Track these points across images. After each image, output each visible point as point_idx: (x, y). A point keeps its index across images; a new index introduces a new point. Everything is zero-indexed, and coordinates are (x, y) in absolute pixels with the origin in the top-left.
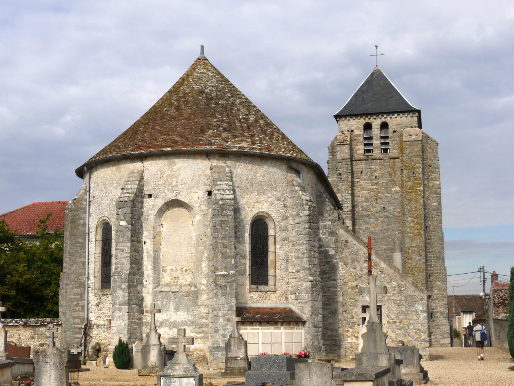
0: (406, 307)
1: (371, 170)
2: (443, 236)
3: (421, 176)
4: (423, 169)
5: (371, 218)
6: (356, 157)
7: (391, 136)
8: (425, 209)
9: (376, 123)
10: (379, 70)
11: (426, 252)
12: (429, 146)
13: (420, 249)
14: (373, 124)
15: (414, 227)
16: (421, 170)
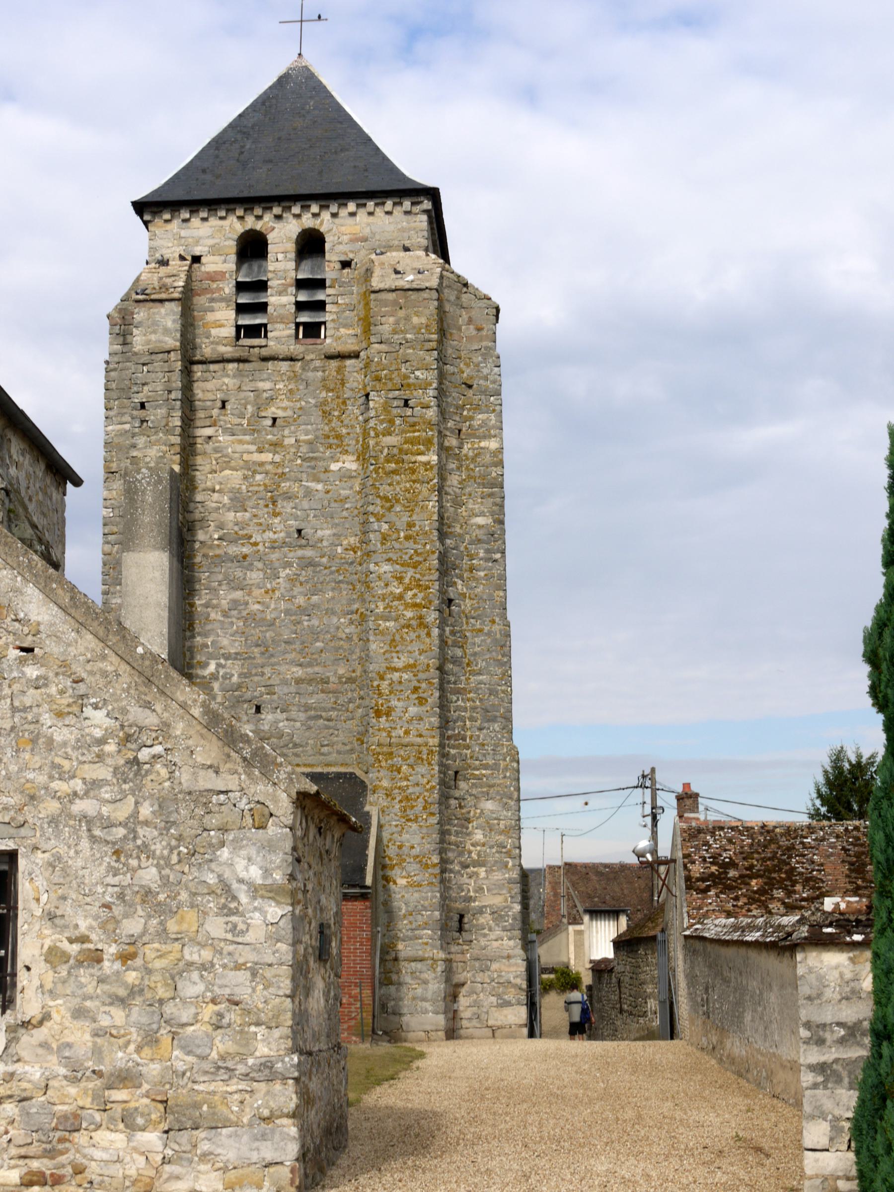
0: (164, 863)
1: (257, 397)
2: (508, 635)
3: (431, 414)
4: (441, 393)
5: (250, 567)
6: (206, 350)
7: (335, 280)
8: (442, 535)
9: (282, 232)
10: (306, 67)
11: (442, 689)
12: (465, 316)
13: (422, 676)
14: (270, 237)
15: (400, 597)
16: (431, 393)
